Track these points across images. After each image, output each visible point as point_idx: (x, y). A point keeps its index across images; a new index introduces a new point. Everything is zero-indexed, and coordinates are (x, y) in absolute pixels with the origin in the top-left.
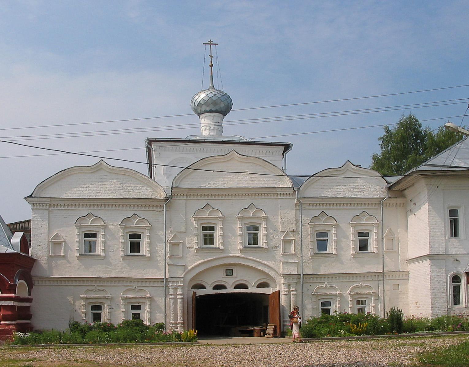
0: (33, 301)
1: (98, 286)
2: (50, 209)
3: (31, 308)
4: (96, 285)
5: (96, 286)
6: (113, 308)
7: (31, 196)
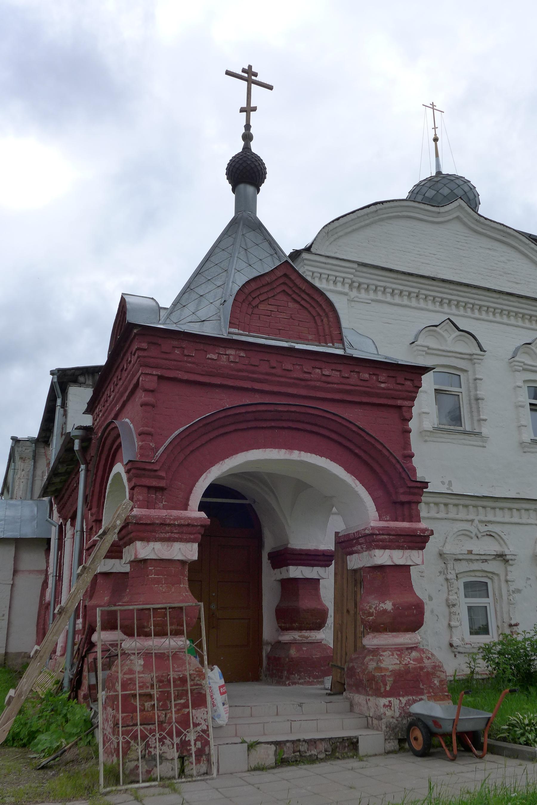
1: (481, 522)
5: (476, 522)
6: (519, 591)
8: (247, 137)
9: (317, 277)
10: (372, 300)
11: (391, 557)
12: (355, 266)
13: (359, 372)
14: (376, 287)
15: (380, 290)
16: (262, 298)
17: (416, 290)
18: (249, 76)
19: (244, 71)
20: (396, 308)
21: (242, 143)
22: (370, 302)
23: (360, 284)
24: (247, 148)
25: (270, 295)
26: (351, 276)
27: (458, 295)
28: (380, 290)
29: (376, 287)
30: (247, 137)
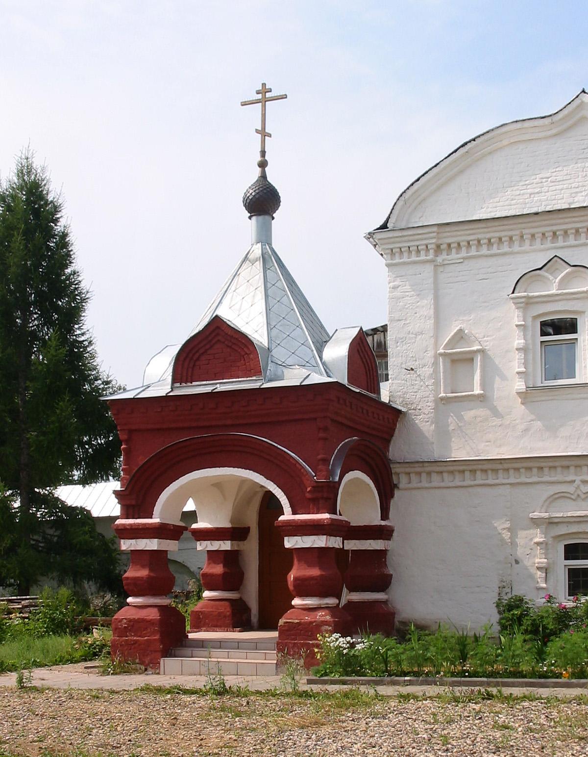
0: (395, 534)
2: (439, 259)
3: (389, 556)
4: (578, 479)
7: (384, 226)
8: (263, 164)
9: (397, 252)
10: (464, 258)
11: (238, 545)
12: (435, 229)
13: (256, 400)
14: (469, 243)
15: (473, 245)
16: (201, 351)
17: (517, 232)
18: (264, 96)
19: (258, 93)
20: (494, 259)
21: (258, 170)
22: (462, 260)
23: (449, 245)
24: (263, 176)
25: (208, 347)
26: (434, 241)
27: (574, 222)
28: (473, 245)
29: (469, 243)
30: (263, 164)
